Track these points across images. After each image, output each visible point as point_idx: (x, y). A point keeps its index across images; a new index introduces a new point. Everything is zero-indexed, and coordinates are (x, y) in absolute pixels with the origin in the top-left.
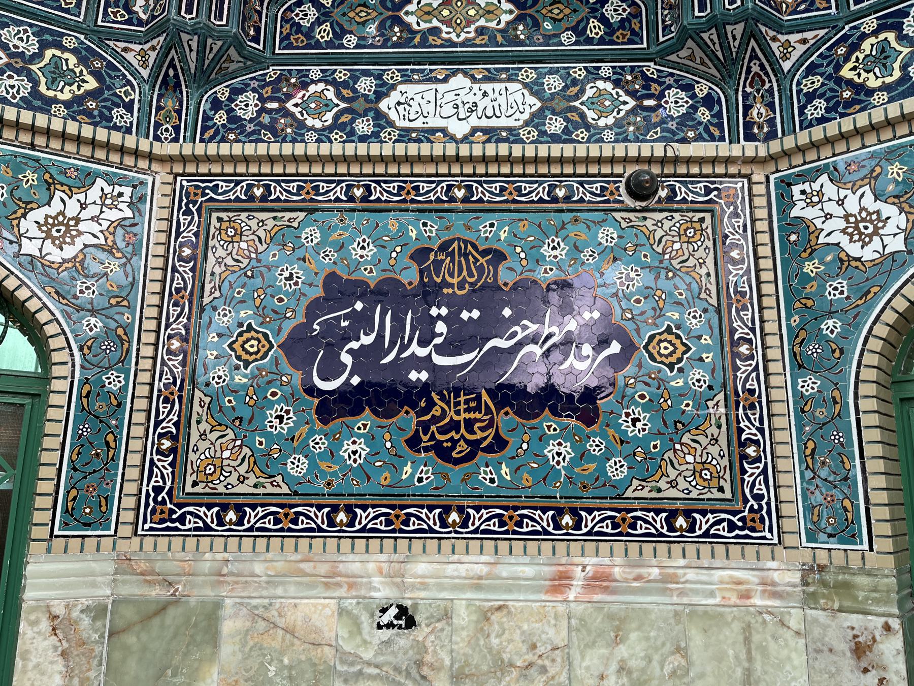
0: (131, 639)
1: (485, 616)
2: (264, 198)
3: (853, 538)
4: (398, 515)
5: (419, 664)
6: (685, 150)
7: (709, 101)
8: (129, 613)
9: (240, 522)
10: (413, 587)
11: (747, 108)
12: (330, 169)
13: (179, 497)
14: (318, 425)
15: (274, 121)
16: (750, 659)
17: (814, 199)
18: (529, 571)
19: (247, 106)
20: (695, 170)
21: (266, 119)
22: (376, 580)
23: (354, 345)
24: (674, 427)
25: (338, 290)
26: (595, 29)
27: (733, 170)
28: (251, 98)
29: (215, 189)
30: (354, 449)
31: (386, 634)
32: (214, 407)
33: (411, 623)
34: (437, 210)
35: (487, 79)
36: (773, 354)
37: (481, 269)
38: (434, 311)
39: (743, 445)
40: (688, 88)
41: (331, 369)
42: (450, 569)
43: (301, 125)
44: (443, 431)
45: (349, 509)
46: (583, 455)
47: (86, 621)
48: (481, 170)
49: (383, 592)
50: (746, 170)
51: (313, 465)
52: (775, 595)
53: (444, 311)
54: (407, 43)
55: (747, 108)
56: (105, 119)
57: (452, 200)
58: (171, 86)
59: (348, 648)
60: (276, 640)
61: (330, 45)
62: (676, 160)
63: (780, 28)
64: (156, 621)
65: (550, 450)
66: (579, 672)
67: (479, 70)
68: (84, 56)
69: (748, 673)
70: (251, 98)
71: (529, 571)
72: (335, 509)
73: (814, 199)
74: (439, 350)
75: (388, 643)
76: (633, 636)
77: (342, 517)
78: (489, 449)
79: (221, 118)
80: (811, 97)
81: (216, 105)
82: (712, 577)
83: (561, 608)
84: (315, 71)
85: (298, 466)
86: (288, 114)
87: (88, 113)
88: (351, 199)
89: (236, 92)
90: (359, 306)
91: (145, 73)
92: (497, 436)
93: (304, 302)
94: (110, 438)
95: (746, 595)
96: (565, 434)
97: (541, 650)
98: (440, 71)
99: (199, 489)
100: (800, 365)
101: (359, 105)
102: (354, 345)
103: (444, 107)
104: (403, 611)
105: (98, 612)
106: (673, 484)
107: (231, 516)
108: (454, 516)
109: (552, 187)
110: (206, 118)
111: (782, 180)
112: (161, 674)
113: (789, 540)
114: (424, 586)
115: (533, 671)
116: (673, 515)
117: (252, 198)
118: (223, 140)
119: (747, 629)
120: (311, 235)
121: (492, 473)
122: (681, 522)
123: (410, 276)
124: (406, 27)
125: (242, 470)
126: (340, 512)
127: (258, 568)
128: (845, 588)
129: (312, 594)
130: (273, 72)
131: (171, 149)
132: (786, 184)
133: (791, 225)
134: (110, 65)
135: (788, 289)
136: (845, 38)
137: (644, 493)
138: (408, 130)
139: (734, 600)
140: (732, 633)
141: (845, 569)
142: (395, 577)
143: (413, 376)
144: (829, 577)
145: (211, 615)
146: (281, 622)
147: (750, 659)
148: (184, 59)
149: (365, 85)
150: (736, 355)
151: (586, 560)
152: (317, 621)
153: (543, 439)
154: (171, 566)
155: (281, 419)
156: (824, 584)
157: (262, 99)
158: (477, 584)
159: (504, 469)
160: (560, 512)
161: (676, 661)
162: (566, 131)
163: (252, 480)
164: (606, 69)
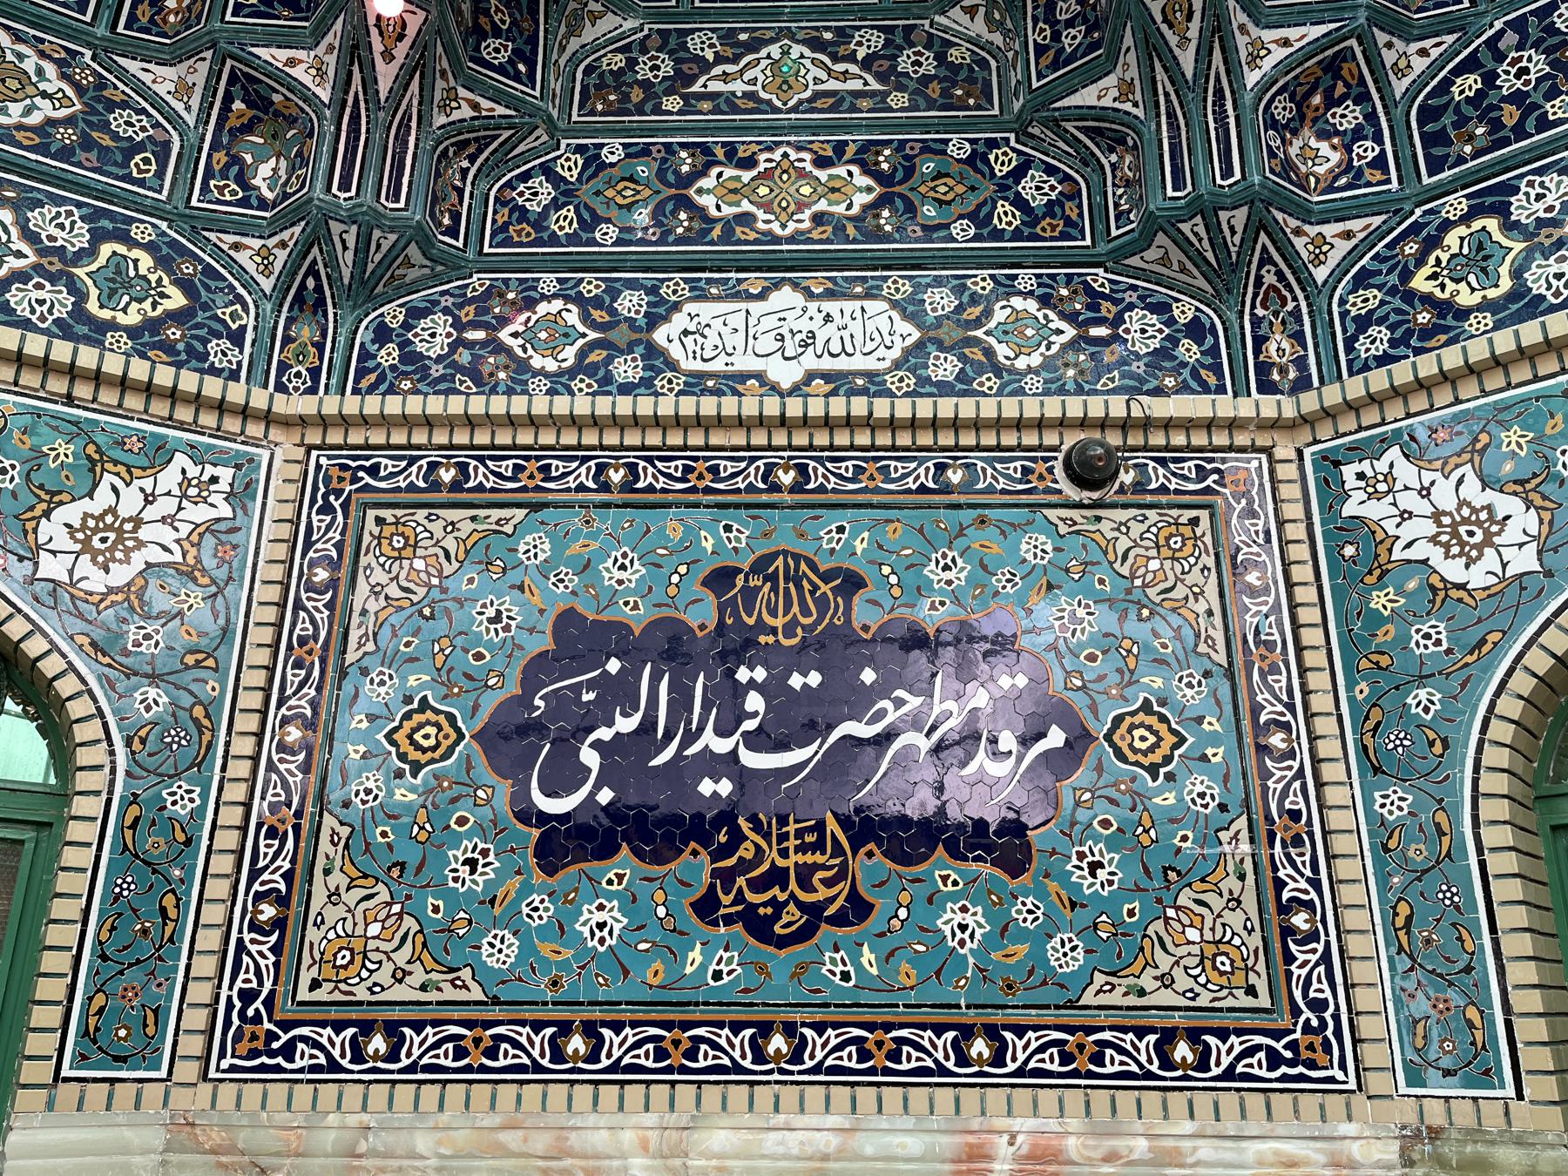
2: (456, 486)
6: (1162, 408)
7: (1196, 330)
11: (1259, 341)
12: (569, 438)
14: (538, 877)
18: (913, 1144)
21: (464, 357)
23: (604, 734)
24: (1164, 878)
26: (1006, 216)
27: (1242, 439)
28: (440, 324)
29: (373, 471)
30: (601, 918)
32: (356, 845)
35: (830, 295)
36: (1324, 748)
37: (822, 603)
38: (743, 675)
39: (1285, 909)
40: (1161, 308)
41: (563, 777)
43: (523, 366)
44: (758, 885)
48: (822, 439)
51: (527, 949)
53: (760, 674)
54: (702, 236)
55: (1259, 341)
56: (195, 357)
57: (775, 488)
58: (308, 304)
61: (573, 239)
62: (1147, 424)
63: (1306, 214)
65: (948, 919)
67: (817, 280)
70: (440, 324)
71: (913, 1144)
72: (565, 1029)
74: (756, 741)
77: (577, 1043)
78: (839, 920)
79: (388, 355)
80: (1363, 323)
81: (382, 334)
84: (548, 282)
89: (415, 313)
90: (614, 666)
91: (267, 284)
94: (169, 901)
96: (973, 891)
98: (754, 281)
99: (321, 995)
101: (620, 335)
102: (604, 734)
106: (1166, 981)
107: (378, 1043)
108: (778, 1043)
110: (365, 355)
113: (1375, 1082)
116: (1168, 1037)
117: (436, 486)
118: (392, 390)
120: (536, 545)
121: (845, 963)
123: (702, 613)
124: (699, 212)
125: (401, 957)
127: (423, 1142)
130: (478, 282)
131: (304, 405)
132: (1331, 462)
133: (1346, 529)
134: (209, 271)
135: (1347, 637)
136: (1415, 228)
137: (1115, 998)
138: (702, 376)
141: (1476, 1133)
143: (706, 787)
148: (332, 263)
149: (631, 303)
155: (473, 866)
157: (459, 325)
159: (867, 955)
162: (961, 377)
163: (418, 977)
164: (1026, 278)
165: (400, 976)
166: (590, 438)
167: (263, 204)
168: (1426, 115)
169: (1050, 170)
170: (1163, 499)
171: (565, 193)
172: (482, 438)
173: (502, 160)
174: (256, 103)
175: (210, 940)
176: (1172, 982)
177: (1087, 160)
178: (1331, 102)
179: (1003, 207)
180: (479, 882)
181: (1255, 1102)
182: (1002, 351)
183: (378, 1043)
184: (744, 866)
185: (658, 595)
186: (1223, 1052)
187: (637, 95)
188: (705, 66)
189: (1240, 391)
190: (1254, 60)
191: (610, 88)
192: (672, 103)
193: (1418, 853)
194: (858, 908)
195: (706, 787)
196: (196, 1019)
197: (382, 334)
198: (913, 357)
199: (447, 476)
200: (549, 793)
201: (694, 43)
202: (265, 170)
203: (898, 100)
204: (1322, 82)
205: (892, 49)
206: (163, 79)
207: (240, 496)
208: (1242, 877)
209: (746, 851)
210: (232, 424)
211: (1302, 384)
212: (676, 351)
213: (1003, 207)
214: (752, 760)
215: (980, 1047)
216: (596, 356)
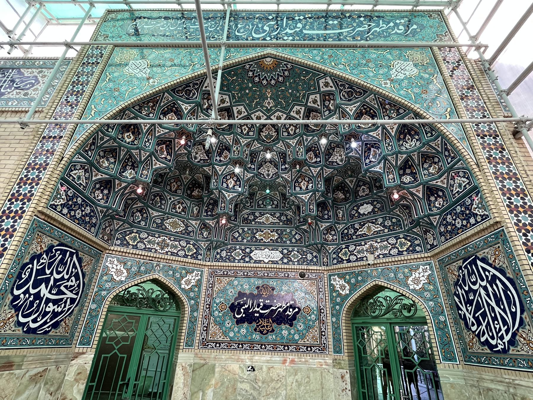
0: (197, 372)
1: (269, 369)
2: (227, 274)
3: (341, 353)
4: (251, 346)
5: (256, 379)
6: (311, 268)
7: (316, 257)
8: (197, 366)
9: (220, 347)
10: (255, 362)
11: (323, 259)
12: (240, 269)
13: (207, 340)
14: (236, 325)
15: (229, 257)
16: (322, 379)
17: (335, 280)
18: (278, 359)
19: (224, 254)
20: (313, 271)
21: (227, 257)
22: (247, 360)
23: (244, 307)
24: (308, 328)
25: (241, 295)
26: (294, 240)
27: (320, 272)
28: (224, 252)
29: (217, 272)
30: (243, 331)
31: (249, 372)
32: (215, 321)
33: (254, 370)
34: (261, 278)
35: (272, 250)
36: (328, 312)
37: (270, 292)
38: (260, 300)
39: (322, 332)
40: (312, 254)
41: (239, 313)
42: (262, 358)
43: (235, 258)
44: (261, 327)
45: (242, 344)
46: (290, 333)
47: (188, 368)
48: (270, 270)
49: (249, 363)
50: (323, 272)
51: (235, 334)
52: (327, 365)
53: (262, 300)
54: (256, 242)
55: (323, 259)
56: (196, 258)
57: (265, 276)
58: (209, 250)
59: (241, 375)
60: (226, 373)
61: (241, 241)
62: (309, 270)
63: (328, 245)
64: (202, 368)
65: (283, 332)
66: (288, 382)
67: (271, 248)
68: (194, 245)
69: (322, 382)
70: (224, 252)
71: (278, 359)
72: (239, 344)
73: (335, 280)
74: (261, 309)
75: (249, 374)
76: (299, 374)
77: (240, 346)
78: (271, 332)
79: (218, 256)
80: (334, 259)
81: (218, 253)
82: (315, 361)
83: (285, 367)
84: (238, 247)
85: (232, 334)
86: (232, 256)
87: (194, 257)
88: (244, 275)
89: (222, 251)
90: (245, 299)
91: (204, 248)
92: (272, 329)
93: (234, 297)
94: (447, 335)
95: (322, 365)
96: (286, 329)
97: (280, 377)
98: (263, 248)
99: (211, 339)
100: (333, 315)
101: (246, 255)
102: (244, 307)
103: (264, 255)
104: (252, 367)
105: (190, 366)
106: (308, 340)
107: (218, 345)
108: (263, 347)
109: (285, 274)
110: (216, 256)
111: (329, 275)
112: (203, 380)
113: (330, 353)
114: (257, 362)
115: (278, 381)
116: (307, 347)
117: (224, 274)
118: (219, 262)
119: (322, 373)
120: (236, 283)
121: (271, 337)
122: (309, 349)
123: (256, 292)
124: (256, 238)
125: (220, 335)
126: (241, 345)
127: (223, 357)
128: (340, 363)
129: (233, 364)
130: (229, 247)
131: (209, 263)
132: (330, 276)
133: (331, 285)
134: (198, 247)
135: (331, 298)
136: (340, 248)
137: (302, 342)
138: (256, 260)
139: (319, 366)
140: (319, 373)
141: (340, 359)
142: (251, 360)
143: (256, 315)
144: (337, 361)
145: (214, 367)
146: (227, 369)
147: (322, 379)
148: (213, 245)
149: (248, 250)
150: (321, 312)
151: (290, 357)
152: (235, 369)
153: (282, 330)
154: (206, 356)
155: (228, 323)
156: (336, 363)
157: (227, 253)
158: (268, 362)
159: (274, 336)
160: (285, 346)
161: (307, 380)
162: (288, 262)
163: (222, 337)
164: (296, 249)
165: (220, 337)
166: (243, 269)
167: (205, 238)
168: (342, 234)
169: (299, 234)
170: (311, 279)
171: (240, 235)
172: (230, 268)
173: (232, 230)
174: (205, 226)
175: (199, 332)
176: (308, 341)
177: (304, 233)
178: (331, 231)
179: (293, 239)
180: (229, 326)
181: (317, 355)
182: (292, 259)
183: (218, 345)
184: (260, 325)
185: (250, 290)
186: (313, 349)
187: (249, 221)
188: (258, 217)
189: (320, 266)
190: (321, 227)
191: (246, 221)
192: (253, 223)
193: (336, 326)
194: (273, 331)
195: (256, 315)
196: (197, 341)
197: (218, 253)
198: (282, 259)
199: (225, 273)
200: (237, 315)
201: (256, 214)
202: (205, 233)
203: (281, 223)
204: (329, 229)
205: (281, 216)
206: (194, 223)
207: (201, 276)
208: (529, 325)
209: (260, 323)
210: (201, 266)
211: (327, 265)
212: (253, 257)
213: (293, 239)
214: (261, 311)
215: (286, 348)
216: (244, 257)
